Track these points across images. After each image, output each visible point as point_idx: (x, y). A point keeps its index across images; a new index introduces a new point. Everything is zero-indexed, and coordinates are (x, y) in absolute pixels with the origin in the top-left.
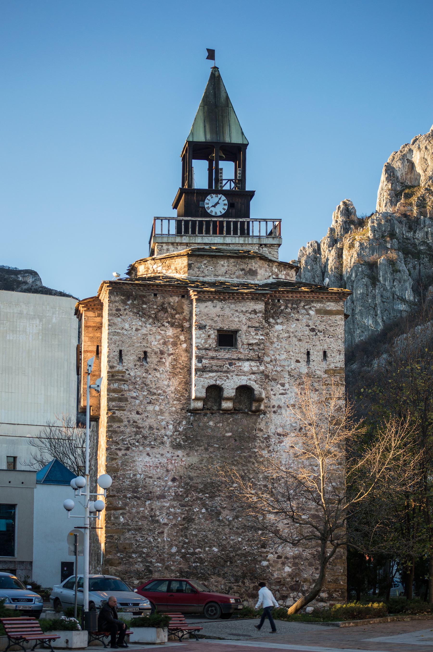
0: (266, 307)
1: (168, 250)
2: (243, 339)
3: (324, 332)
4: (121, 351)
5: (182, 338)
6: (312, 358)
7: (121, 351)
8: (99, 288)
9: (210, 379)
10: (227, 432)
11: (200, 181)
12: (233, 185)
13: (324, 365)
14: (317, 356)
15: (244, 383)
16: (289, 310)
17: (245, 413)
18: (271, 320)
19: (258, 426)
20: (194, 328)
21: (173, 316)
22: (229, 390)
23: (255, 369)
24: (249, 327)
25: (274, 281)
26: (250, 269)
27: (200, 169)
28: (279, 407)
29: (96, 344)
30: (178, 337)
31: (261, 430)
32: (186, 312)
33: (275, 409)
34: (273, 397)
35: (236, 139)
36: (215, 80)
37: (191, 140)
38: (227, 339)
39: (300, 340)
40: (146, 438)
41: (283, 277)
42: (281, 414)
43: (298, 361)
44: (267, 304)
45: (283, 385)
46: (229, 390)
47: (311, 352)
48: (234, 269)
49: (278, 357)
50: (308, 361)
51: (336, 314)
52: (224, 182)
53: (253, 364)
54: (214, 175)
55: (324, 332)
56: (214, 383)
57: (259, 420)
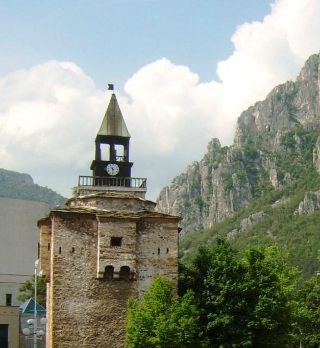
0: (137, 226)
1: (86, 193)
2: (124, 241)
3: (167, 238)
4: (60, 248)
5: (93, 241)
6: (160, 252)
7: (60, 248)
8: (78, 179)
9: (108, 263)
10: (116, 290)
11: (105, 156)
12: (122, 159)
13: (167, 256)
14: (163, 251)
15: (125, 265)
16: (149, 227)
17: (125, 280)
18: (140, 232)
19: (132, 287)
20: (99, 236)
21: (88, 229)
22: (117, 269)
23: (131, 257)
24: (128, 236)
25: (143, 211)
26: (130, 205)
27: (105, 148)
28: (144, 277)
29: (48, 242)
30: (90, 240)
31: (134, 289)
32: (95, 228)
33: (141, 278)
34: (140, 272)
35: (124, 135)
36: (114, 100)
37: (100, 134)
38: (116, 242)
39: (155, 243)
40: (73, 293)
41: (148, 209)
42: (144, 281)
43: (153, 254)
44: (137, 224)
45: (145, 266)
46: (117, 269)
47: (160, 249)
48: (121, 205)
49: (143, 251)
50: (159, 253)
51: (174, 229)
52: (117, 158)
53: (130, 255)
54: (113, 152)
55: (167, 238)
56: (109, 265)
57: (133, 284)
